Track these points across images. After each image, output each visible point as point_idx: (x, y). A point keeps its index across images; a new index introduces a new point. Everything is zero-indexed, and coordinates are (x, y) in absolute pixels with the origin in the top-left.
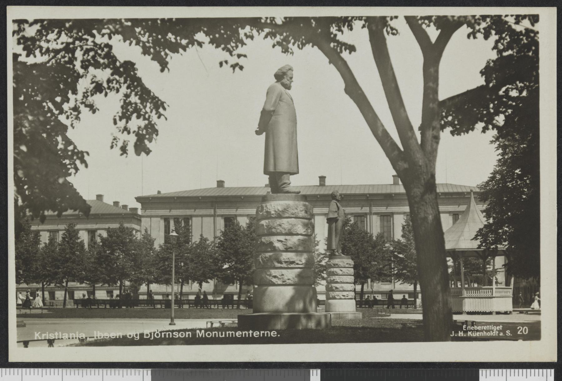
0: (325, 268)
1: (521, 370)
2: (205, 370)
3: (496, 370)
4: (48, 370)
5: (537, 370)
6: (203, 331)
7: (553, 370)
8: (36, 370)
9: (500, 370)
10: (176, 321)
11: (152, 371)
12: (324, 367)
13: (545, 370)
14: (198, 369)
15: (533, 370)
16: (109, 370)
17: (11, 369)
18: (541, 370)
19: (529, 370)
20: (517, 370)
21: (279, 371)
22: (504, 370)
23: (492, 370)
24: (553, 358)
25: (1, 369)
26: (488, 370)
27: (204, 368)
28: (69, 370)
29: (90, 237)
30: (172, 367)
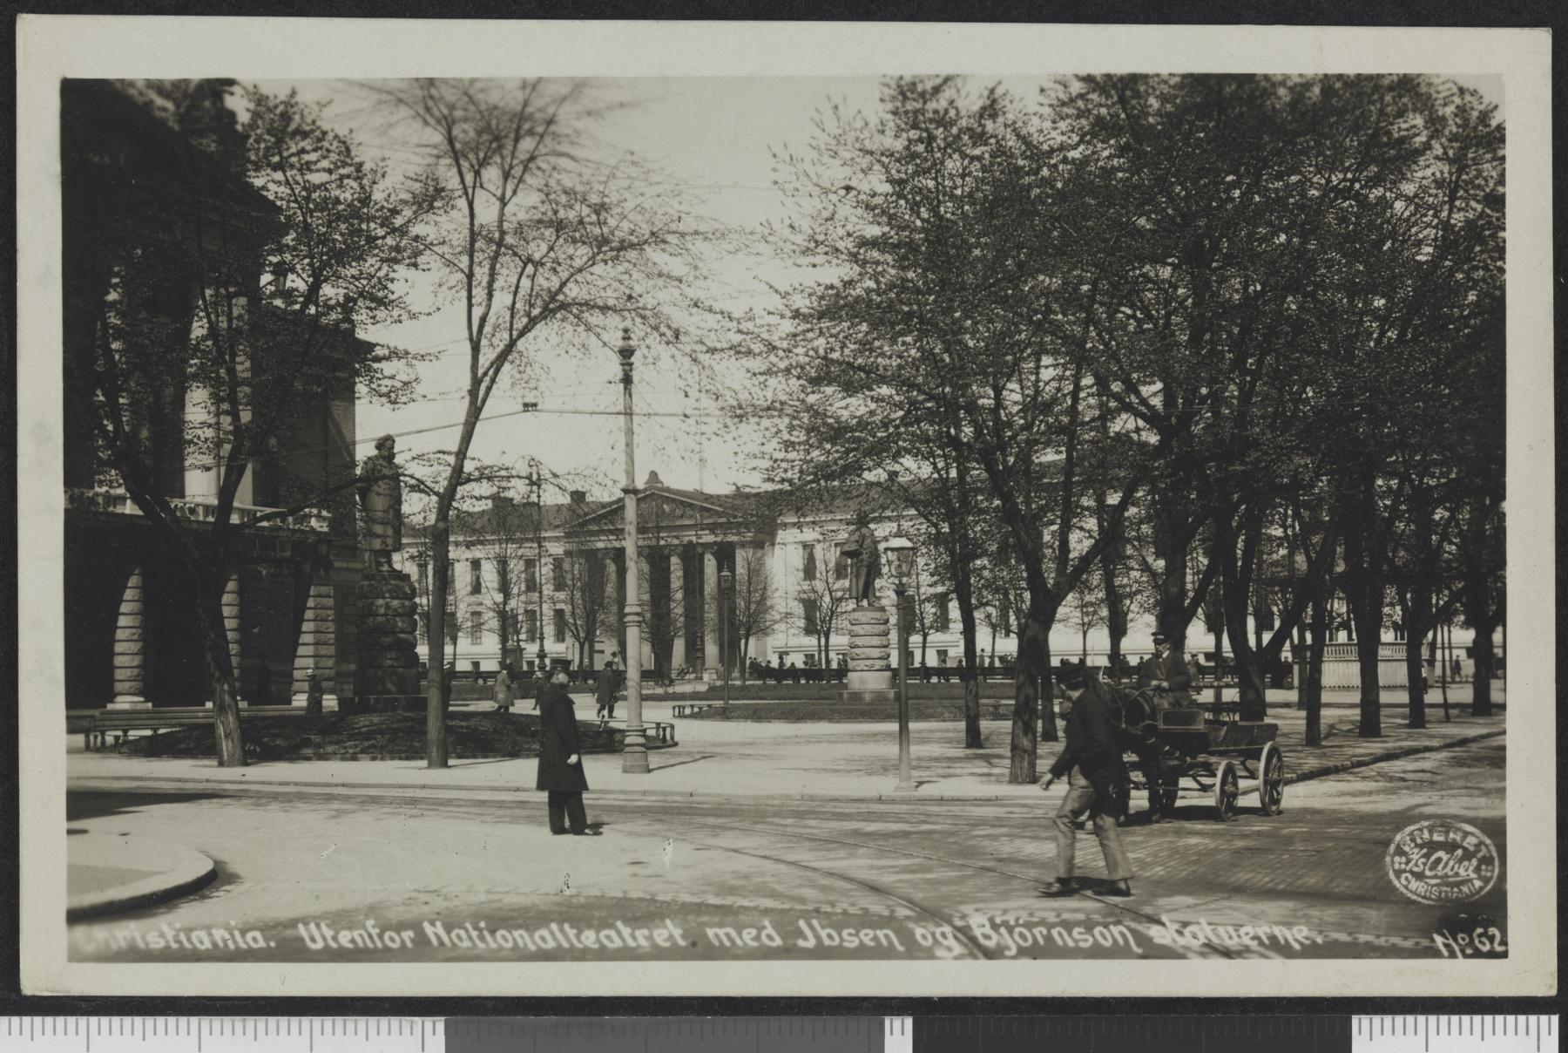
7: (1555, 1019)
11: (446, 1022)
21: (797, 1021)
24: (1546, 986)
25: (4, 1020)
29: (1348, 76)
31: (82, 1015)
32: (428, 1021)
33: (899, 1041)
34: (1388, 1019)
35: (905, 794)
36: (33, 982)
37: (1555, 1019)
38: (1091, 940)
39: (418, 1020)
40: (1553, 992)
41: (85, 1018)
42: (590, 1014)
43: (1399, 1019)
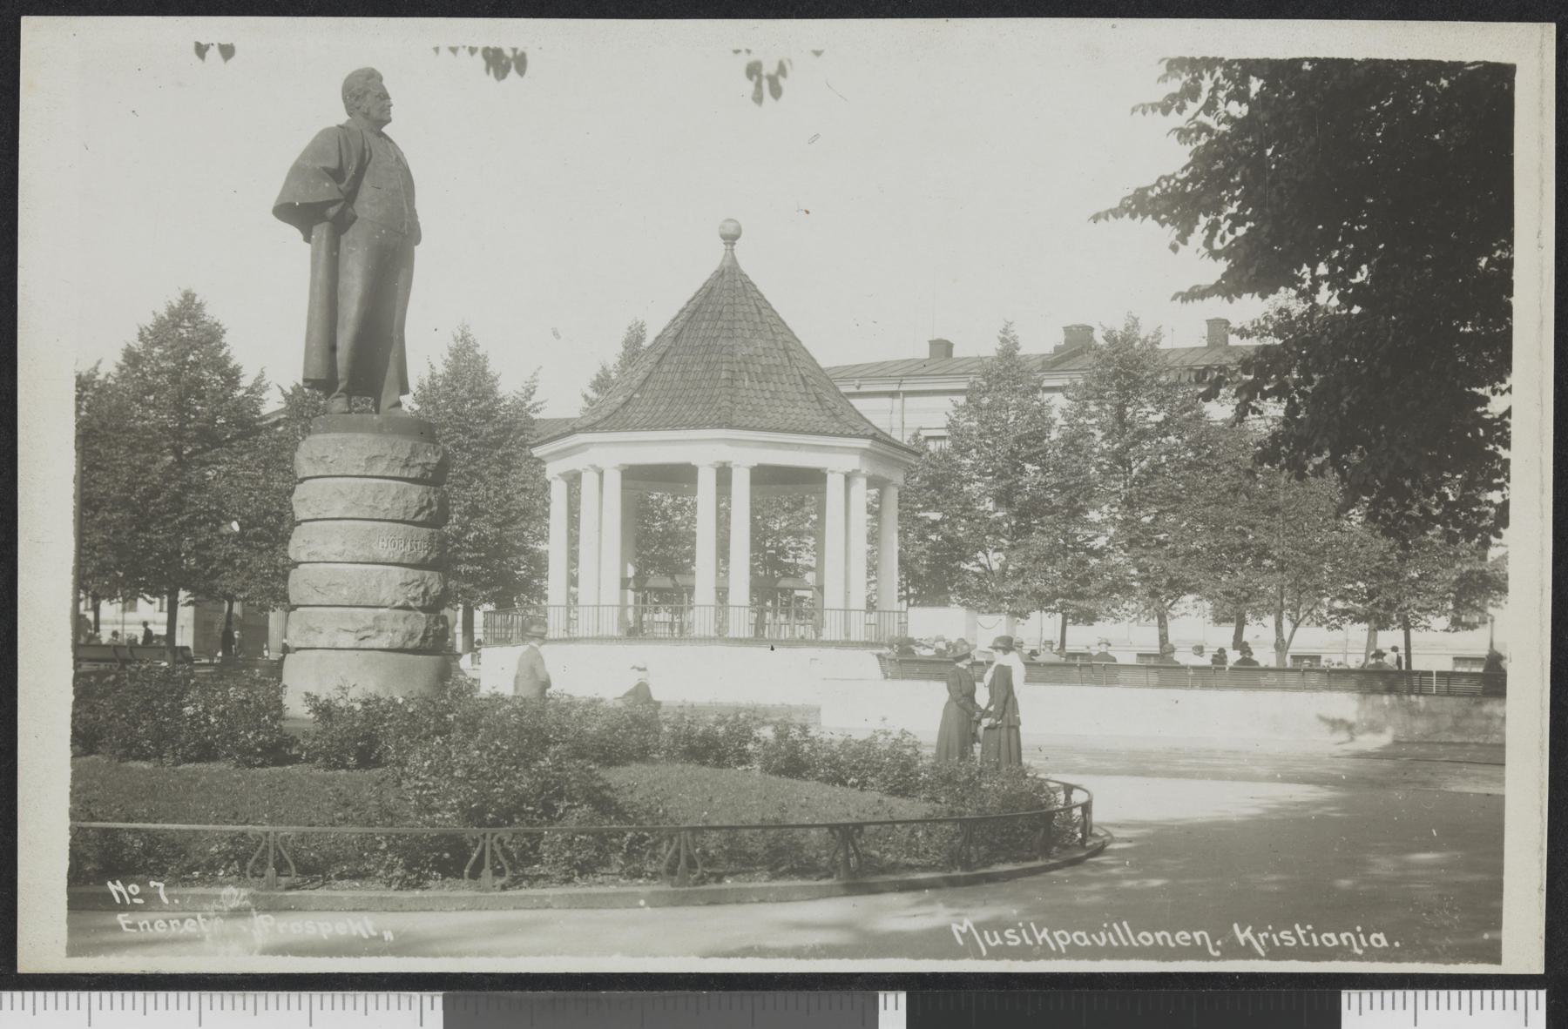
4: (161, 995)
7: (1543, 994)
8: (184, 995)
11: (444, 996)
14: (572, 993)
16: (327, 995)
17: (26, 993)
21: (792, 995)
24: (1538, 968)
25: (6, 995)
31: (84, 989)
32: (427, 996)
33: (892, 1017)
34: (1377, 994)
35: (595, 890)
36: (29, 961)
37: (1543, 994)
38: (1019, 941)
39: (416, 995)
40: (1543, 972)
41: (87, 993)
42: (587, 989)
43: (1388, 994)
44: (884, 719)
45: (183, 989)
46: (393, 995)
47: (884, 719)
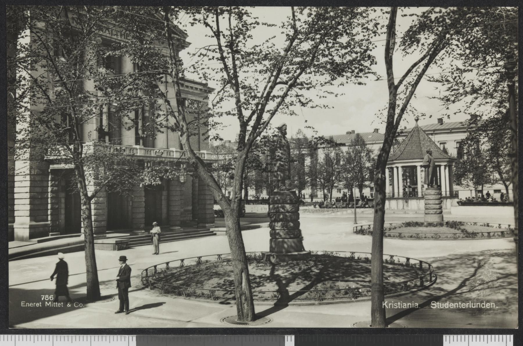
0: (196, 116)
1: (482, 336)
2: (187, 336)
3: (459, 336)
4: (40, 336)
5: (497, 336)
6: (50, 303)
7: (512, 336)
8: (47, 336)
9: (463, 336)
10: (164, 247)
12: (297, 332)
13: (504, 336)
14: (180, 335)
15: (493, 336)
16: (97, 336)
18: (501, 336)
19: (489, 336)
20: (478, 336)
21: (255, 336)
22: (467, 336)
23: (455, 336)
25: (2, 336)
26: (452, 336)
27: (185, 334)
28: (97, 336)
30: (207, 334)
31: (13, 334)
44: (306, 121)
45: (47, 334)
46: (119, 336)
47: (306, 121)
